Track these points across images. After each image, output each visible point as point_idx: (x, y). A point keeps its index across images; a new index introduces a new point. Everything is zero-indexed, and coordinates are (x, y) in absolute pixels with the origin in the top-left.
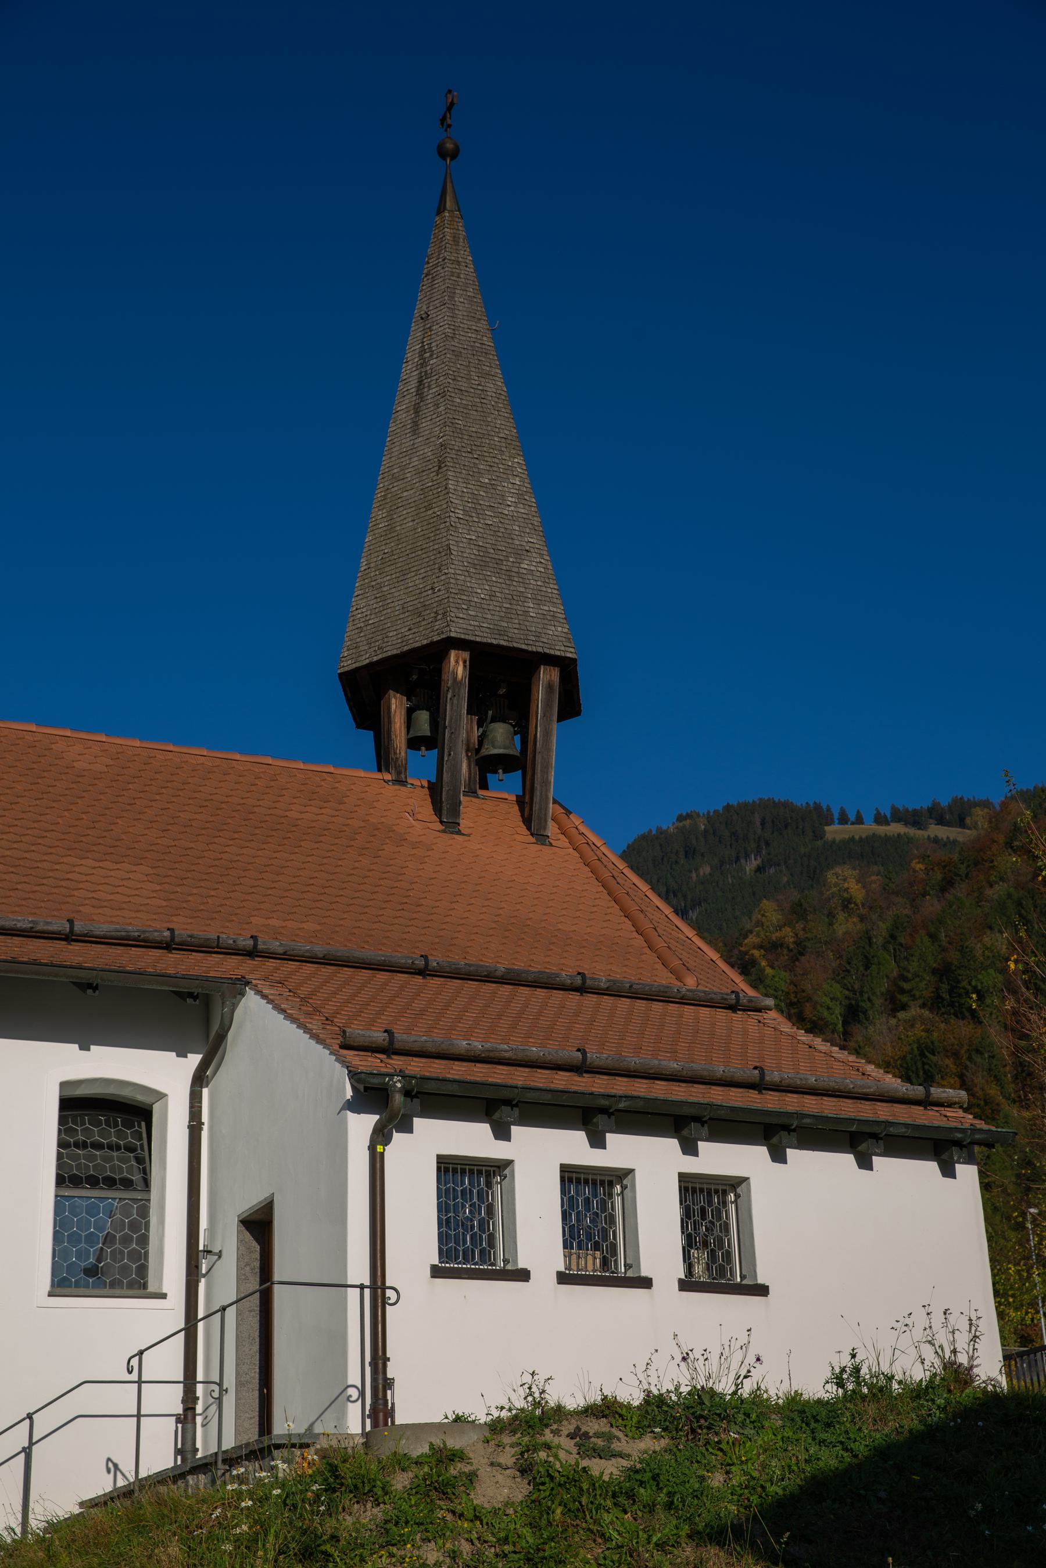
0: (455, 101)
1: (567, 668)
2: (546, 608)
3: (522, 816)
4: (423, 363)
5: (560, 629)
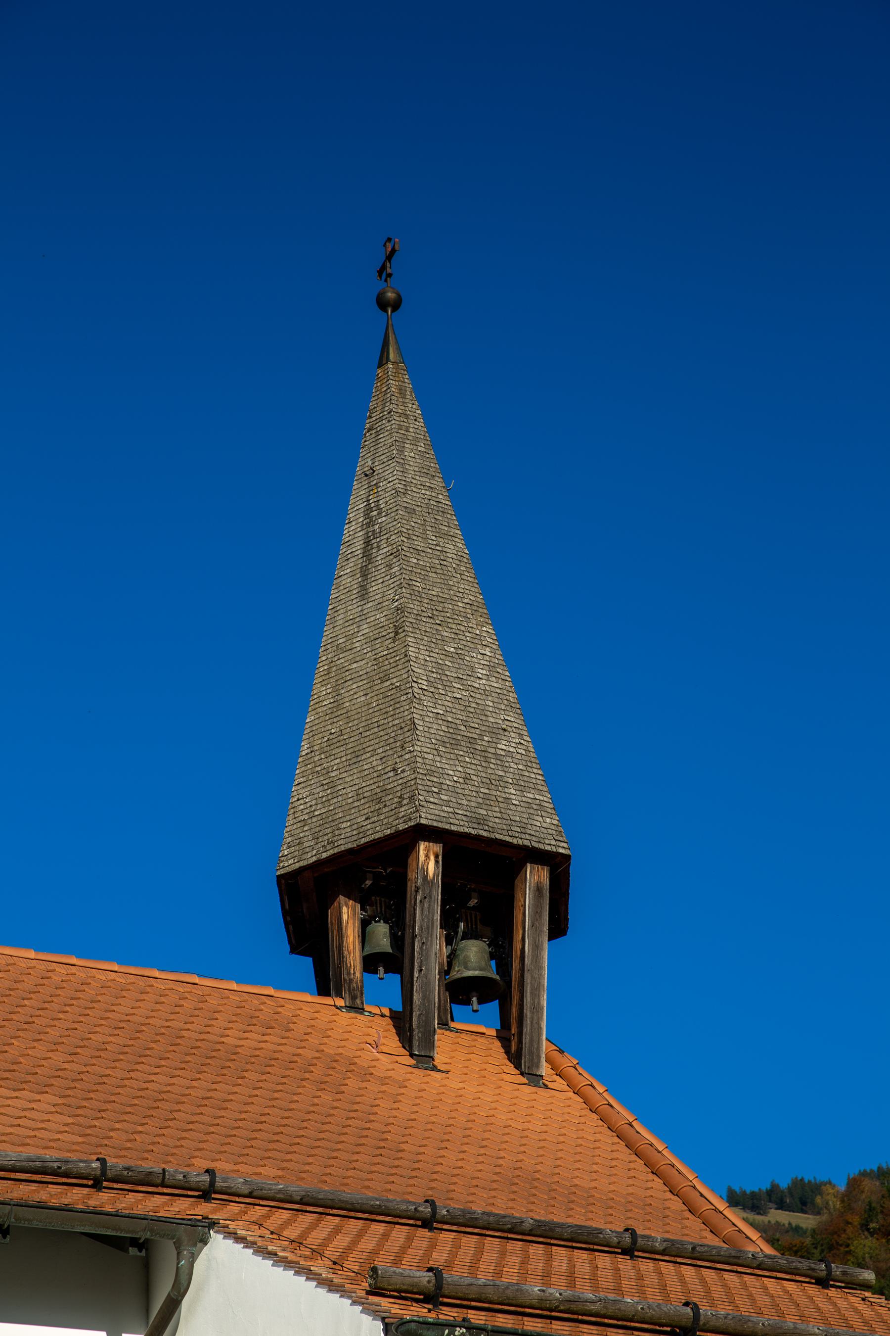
0: (397, 247)
1: (557, 865)
2: (531, 796)
3: (508, 1052)
4: (370, 521)
5: (548, 820)
